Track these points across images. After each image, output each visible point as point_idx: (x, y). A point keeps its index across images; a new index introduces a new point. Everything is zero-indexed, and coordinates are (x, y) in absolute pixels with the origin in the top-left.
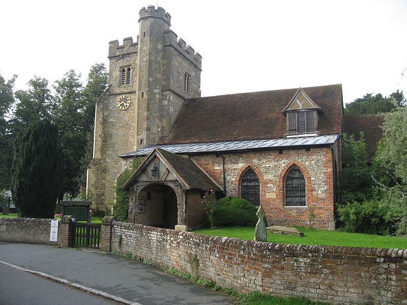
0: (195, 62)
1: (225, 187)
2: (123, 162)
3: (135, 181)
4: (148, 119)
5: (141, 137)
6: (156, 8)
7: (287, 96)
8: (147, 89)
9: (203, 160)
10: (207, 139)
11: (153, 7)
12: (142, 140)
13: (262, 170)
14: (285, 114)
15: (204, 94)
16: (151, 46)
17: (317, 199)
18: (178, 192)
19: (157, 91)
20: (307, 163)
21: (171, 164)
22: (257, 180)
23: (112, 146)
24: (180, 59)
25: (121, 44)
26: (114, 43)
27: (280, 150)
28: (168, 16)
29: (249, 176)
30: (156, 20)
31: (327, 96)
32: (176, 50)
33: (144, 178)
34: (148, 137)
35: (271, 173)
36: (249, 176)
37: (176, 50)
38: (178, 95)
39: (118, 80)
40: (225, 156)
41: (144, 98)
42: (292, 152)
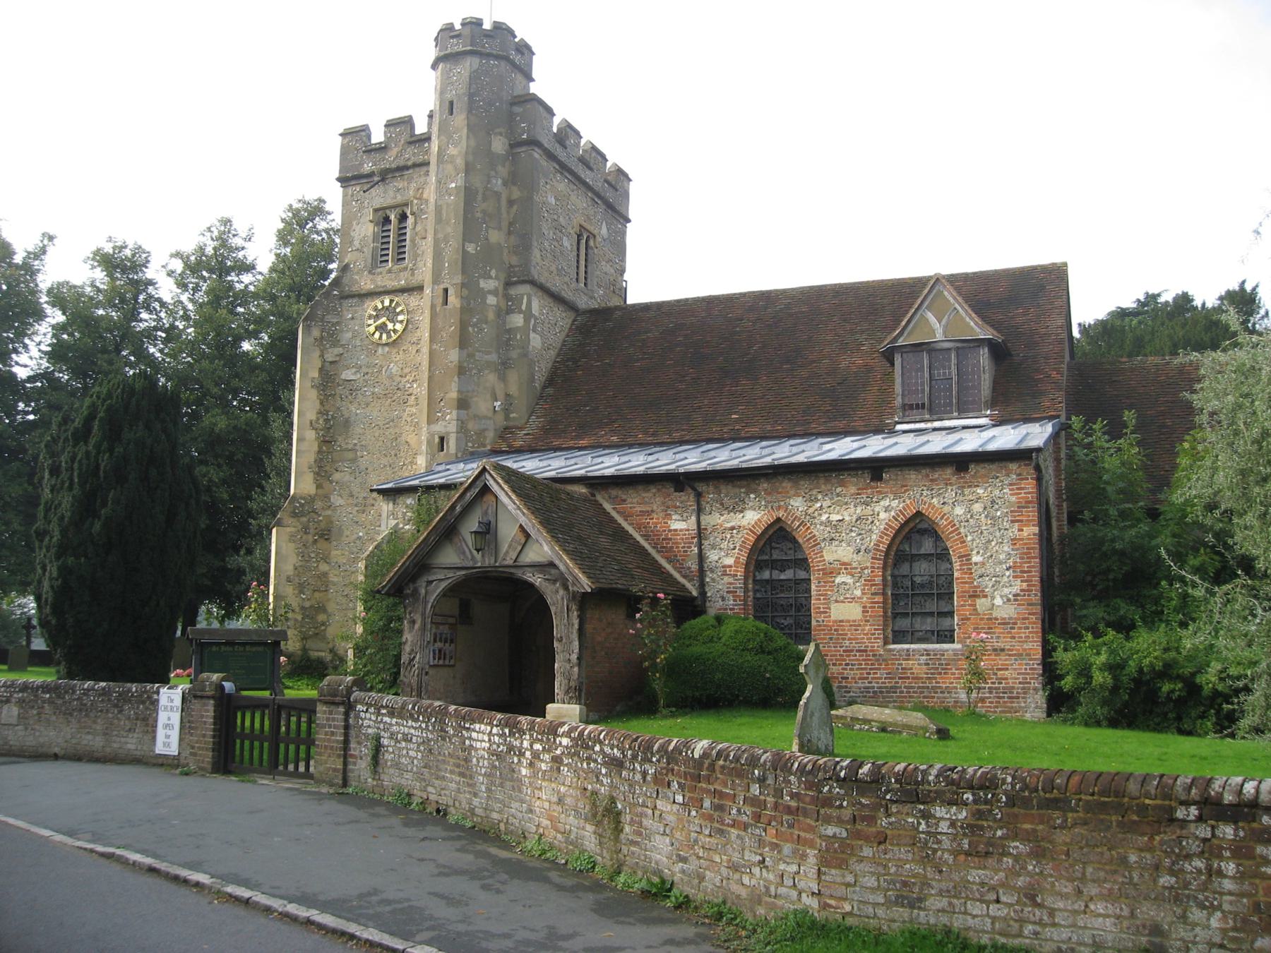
0: (610, 195)
1: (702, 585)
3: (420, 565)
4: (461, 371)
5: (439, 428)
7: (901, 296)
8: (458, 279)
12: (442, 439)
13: (819, 531)
14: (889, 355)
16: (473, 143)
18: (556, 599)
20: (959, 511)
21: (535, 511)
22: (803, 563)
23: (350, 455)
24: (562, 185)
27: (876, 469)
32: (551, 156)
33: (449, 557)
34: (462, 428)
37: (551, 156)
38: (557, 298)
39: (368, 252)
40: (701, 487)
41: (450, 306)
42: (912, 476)
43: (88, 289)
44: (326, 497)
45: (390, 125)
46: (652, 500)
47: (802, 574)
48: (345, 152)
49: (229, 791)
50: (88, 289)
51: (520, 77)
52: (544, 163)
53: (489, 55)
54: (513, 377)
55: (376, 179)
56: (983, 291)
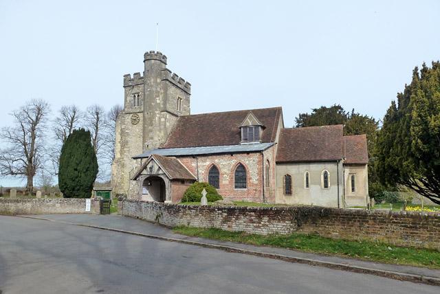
0: (186, 89)
2: (135, 161)
3: (139, 174)
6: (156, 53)
7: (242, 115)
9: (185, 160)
10: (423, 264)
11: (147, 53)
13: (221, 166)
14: (240, 128)
15: (192, 113)
17: (253, 185)
18: (166, 181)
19: (157, 112)
20: (247, 162)
21: (162, 164)
22: (218, 173)
24: (173, 88)
25: (132, 77)
26: (146, 54)
27: (231, 154)
28: (164, 57)
29: (214, 172)
30: (154, 60)
31: (270, 116)
32: (171, 82)
33: (145, 172)
35: (226, 166)
36: (214, 172)
37: (171, 82)
38: (173, 114)
42: (239, 155)
43: (314, 113)
44: (123, 158)
45: (135, 74)
46: (189, 160)
47: (211, 175)
48: (125, 80)
49: (102, 215)
50: (314, 113)
51: (163, 65)
52: (169, 84)
53: (156, 60)
54: (162, 132)
55: (118, 156)
56: (260, 114)
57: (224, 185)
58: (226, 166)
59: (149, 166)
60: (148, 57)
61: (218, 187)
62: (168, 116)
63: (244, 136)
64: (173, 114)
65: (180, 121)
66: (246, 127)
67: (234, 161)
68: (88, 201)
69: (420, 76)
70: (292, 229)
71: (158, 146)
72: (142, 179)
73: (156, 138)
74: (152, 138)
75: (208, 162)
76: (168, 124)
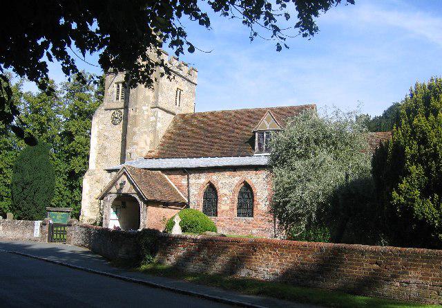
14: (254, 132)
18: (141, 203)
29: (211, 194)
35: (228, 186)
36: (211, 194)
57: (223, 211)
58: (228, 186)
59: (119, 182)
60: (316, 29)
61: (216, 214)
62: (160, 113)
63: (260, 145)
64: (168, 112)
65: (175, 122)
66: (261, 133)
67: (235, 180)
68: (38, 223)
69: (102, 51)
70: (290, 275)
71: (144, 154)
72: (111, 198)
73: (142, 144)
74: (137, 144)
75: (203, 179)
76: (159, 125)
